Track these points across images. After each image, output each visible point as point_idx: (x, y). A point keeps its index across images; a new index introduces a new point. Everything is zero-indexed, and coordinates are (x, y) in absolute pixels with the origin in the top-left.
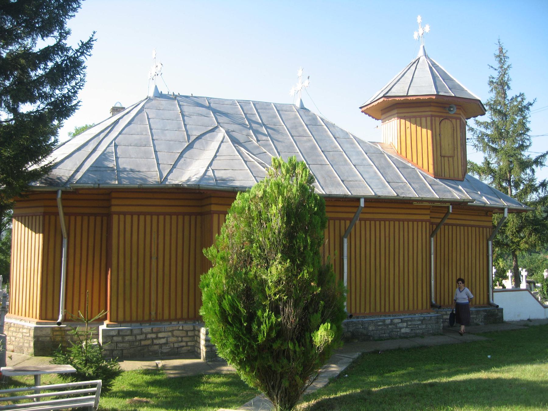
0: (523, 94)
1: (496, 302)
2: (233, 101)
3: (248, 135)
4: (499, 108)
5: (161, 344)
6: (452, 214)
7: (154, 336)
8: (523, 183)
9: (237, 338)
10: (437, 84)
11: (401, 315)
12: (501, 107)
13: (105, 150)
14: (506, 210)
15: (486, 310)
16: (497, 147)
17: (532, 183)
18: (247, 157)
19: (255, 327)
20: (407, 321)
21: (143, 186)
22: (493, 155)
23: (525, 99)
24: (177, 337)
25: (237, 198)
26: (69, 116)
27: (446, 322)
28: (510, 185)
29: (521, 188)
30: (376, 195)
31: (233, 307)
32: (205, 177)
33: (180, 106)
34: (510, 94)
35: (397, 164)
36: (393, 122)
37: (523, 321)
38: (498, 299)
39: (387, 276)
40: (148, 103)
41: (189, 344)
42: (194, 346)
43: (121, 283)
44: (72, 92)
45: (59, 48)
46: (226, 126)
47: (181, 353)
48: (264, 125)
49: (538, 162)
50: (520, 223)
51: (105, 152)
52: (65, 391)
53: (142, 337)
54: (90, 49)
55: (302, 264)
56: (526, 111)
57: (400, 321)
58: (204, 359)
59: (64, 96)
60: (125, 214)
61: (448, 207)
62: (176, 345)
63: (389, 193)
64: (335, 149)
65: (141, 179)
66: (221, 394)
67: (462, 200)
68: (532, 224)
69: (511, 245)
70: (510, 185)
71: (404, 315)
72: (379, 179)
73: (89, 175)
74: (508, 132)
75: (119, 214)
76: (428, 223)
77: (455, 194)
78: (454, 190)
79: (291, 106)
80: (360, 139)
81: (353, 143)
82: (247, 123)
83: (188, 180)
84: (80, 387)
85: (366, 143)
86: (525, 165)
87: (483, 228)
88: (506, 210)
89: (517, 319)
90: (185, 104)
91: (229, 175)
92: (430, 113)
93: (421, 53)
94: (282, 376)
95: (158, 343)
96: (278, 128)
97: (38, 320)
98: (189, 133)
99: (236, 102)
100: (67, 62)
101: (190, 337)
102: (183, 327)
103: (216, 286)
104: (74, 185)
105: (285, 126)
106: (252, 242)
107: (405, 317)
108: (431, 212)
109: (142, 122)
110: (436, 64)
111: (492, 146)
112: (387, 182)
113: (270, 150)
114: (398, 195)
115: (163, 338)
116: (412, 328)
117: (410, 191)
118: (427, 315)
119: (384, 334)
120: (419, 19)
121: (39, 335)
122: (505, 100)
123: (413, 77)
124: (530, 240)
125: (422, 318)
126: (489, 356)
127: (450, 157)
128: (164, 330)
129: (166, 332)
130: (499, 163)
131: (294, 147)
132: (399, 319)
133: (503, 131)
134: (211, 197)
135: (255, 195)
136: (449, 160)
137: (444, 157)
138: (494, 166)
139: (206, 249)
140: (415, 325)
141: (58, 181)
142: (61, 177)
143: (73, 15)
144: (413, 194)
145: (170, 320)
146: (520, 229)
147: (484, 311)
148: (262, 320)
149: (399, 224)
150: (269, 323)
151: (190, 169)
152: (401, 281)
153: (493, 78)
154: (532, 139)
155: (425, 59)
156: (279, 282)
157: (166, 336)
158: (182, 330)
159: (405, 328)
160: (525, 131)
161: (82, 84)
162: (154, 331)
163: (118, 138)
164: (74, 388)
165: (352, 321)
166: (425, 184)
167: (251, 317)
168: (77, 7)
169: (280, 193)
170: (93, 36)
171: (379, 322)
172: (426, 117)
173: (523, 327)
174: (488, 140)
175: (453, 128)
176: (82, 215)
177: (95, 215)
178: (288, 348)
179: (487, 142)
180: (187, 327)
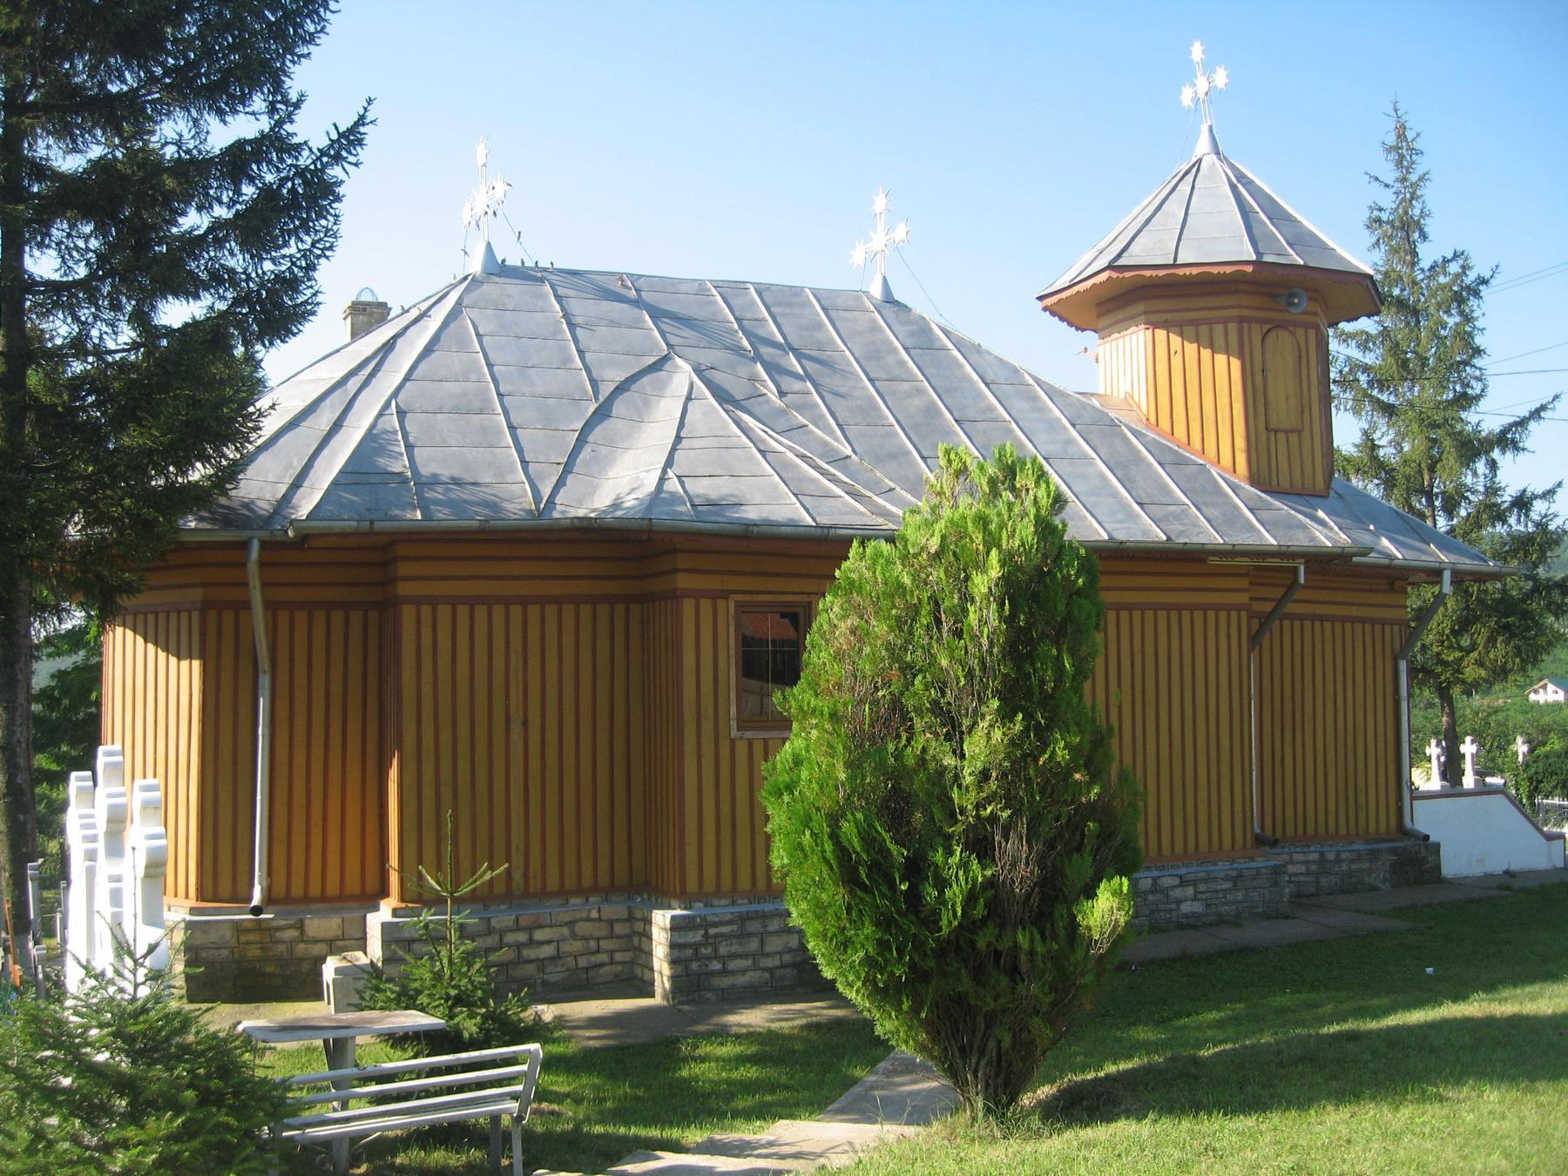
0: (1462, 253)
2: (701, 283)
3: (754, 379)
4: (1396, 292)
5: (542, 960)
6: (1304, 587)
7: (522, 937)
8: (1467, 498)
9: (884, 922)
11: (1178, 867)
14: (1447, 576)
17: (1493, 500)
18: (763, 441)
19: (931, 893)
20: (1194, 883)
22: (1382, 422)
23: (1470, 268)
25: (850, 555)
26: (289, 333)
28: (1431, 504)
29: (1463, 513)
30: (1111, 539)
31: (870, 840)
32: (663, 495)
33: (558, 297)
34: (1428, 254)
35: (1157, 453)
36: (1134, 336)
38: (1423, 819)
40: (472, 291)
41: (618, 957)
42: (631, 963)
43: (428, 793)
44: (300, 268)
45: (274, 143)
46: (688, 351)
48: (792, 349)
49: (1507, 439)
54: (358, 148)
56: (1473, 302)
57: (1176, 881)
58: (665, 996)
60: (433, 602)
61: (1295, 571)
62: (583, 962)
63: (1146, 532)
64: (989, 415)
65: (485, 504)
66: (748, 1087)
67: (1340, 550)
68: (1498, 611)
69: (1439, 669)
70: (1431, 504)
73: (340, 496)
74: (1424, 361)
75: (417, 601)
76: (1244, 614)
77: (1318, 534)
79: (858, 295)
80: (1052, 387)
81: (1034, 398)
82: (745, 343)
83: (616, 505)
84: (450, 1069)
85: (1068, 396)
86: (1473, 448)
87: (1313, 622)
88: (1447, 576)
89: (1477, 870)
90: (571, 293)
91: (725, 491)
92: (1236, 312)
93: (1203, 146)
94: (990, 1019)
95: (533, 956)
97: (192, 902)
98: (595, 375)
104: (304, 524)
106: (909, 670)
107: (1190, 870)
109: (463, 344)
110: (1246, 177)
111: (1378, 399)
112: (1138, 503)
113: (818, 420)
114: (1169, 539)
118: (1246, 866)
120: (1197, 52)
121: (198, 942)
122: (1413, 271)
123: (1186, 214)
124: (1492, 656)
125: (1234, 873)
126: (1429, 970)
127: (1292, 431)
130: (1399, 444)
131: (878, 409)
133: (1409, 355)
134: (674, 551)
136: (1288, 441)
137: (1276, 432)
138: (1386, 452)
139: (783, 693)
140: (1217, 891)
141: (246, 512)
142: (252, 502)
143: (306, 51)
144: (1212, 537)
145: (563, 893)
146: (1464, 624)
147: (1393, 851)
148: (945, 874)
150: (967, 883)
151: (611, 474)
152: (1177, 772)
153: (1380, 210)
154: (1492, 382)
155: (1217, 163)
157: (556, 938)
158: (599, 920)
160: (1472, 356)
161: (328, 245)
162: (522, 923)
163: (403, 391)
166: (1236, 507)
167: (916, 868)
168: (317, 32)
169: (992, 542)
170: (365, 109)
172: (1225, 322)
174: (1369, 382)
177: (347, 606)
178: (1016, 946)
179: (1365, 386)
180: (609, 911)
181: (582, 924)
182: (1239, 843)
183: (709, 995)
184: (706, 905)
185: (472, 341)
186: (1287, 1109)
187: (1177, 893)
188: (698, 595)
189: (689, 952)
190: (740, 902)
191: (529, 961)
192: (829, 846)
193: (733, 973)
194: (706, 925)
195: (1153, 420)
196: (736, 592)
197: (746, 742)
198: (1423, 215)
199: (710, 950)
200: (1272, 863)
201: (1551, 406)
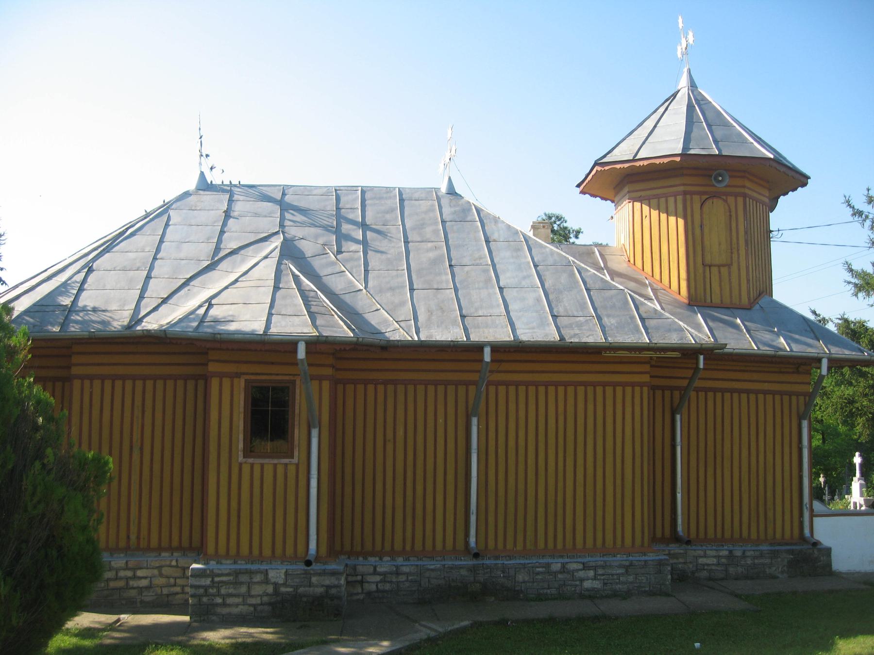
1: (819, 535)
5: (141, 588)
7: (129, 574)
20: (595, 568)
24: (168, 577)
27: (704, 569)
39: (560, 484)
47: (173, 605)
51: (69, 282)
57: (581, 566)
60: (91, 378)
62: (165, 591)
65: (103, 323)
71: (592, 557)
75: (82, 378)
76: (645, 389)
91: (226, 314)
92: (681, 188)
93: (684, 82)
96: (387, 229)
102: (177, 561)
115: (145, 578)
116: (606, 581)
119: (549, 589)
123: (655, 126)
125: (627, 563)
126: (697, 645)
127: (723, 266)
128: (145, 565)
129: (151, 568)
132: (579, 562)
136: (720, 272)
137: (710, 266)
140: (612, 575)
145: (160, 549)
147: (791, 552)
157: (150, 575)
158: (177, 566)
159: (592, 579)
162: (130, 565)
165: (483, 564)
171: (538, 567)
172: (675, 195)
175: (728, 214)
181: (166, 568)
182: (638, 542)
183: (214, 618)
184: (217, 563)
187: (582, 574)
188: (221, 376)
189: (202, 591)
190: (239, 562)
191: (134, 588)
193: (229, 605)
194: (213, 575)
195: (632, 261)
196: (244, 374)
197: (249, 466)
199: (215, 590)
200: (657, 558)
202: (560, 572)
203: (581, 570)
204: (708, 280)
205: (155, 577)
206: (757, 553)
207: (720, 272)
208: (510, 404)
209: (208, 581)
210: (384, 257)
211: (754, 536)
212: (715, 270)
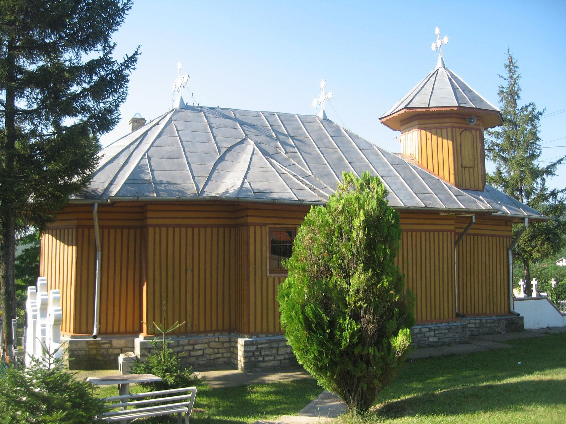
2: (258, 112)
3: (276, 147)
4: (509, 117)
6: (475, 224)
7: (191, 348)
8: (534, 192)
9: (321, 344)
10: (458, 96)
12: (511, 117)
13: (139, 163)
14: (526, 220)
15: (507, 319)
16: (507, 156)
18: (280, 170)
20: (434, 330)
21: (182, 198)
22: (503, 164)
23: (535, 109)
24: (213, 348)
25: (310, 211)
28: (521, 194)
29: (533, 197)
30: (405, 205)
31: (316, 315)
32: (243, 189)
33: (206, 117)
34: (520, 104)
35: (421, 175)
36: (414, 132)
37: (542, 329)
38: (517, 308)
41: (225, 355)
43: (157, 295)
44: (114, 106)
45: (105, 61)
46: (253, 137)
48: (290, 136)
49: (549, 171)
50: (532, 232)
51: (140, 165)
52: (143, 400)
53: (180, 349)
54: (135, 63)
55: (382, 272)
56: (536, 121)
57: (428, 330)
59: (106, 109)
60: (160, 226)
61: (471, 218)
62: (212, 357)
63: (417, 203)
64: (361, 161)
65: (179, 191)
66: (271, 403)
67: (488, 211)
69: (524, 254)
70: (521, 194)
72: (406, 190)
73: (127, 188)
75: (155, 226)
76: (453, 233)
77: (480, 204)
78: (478, 201)
79: (315, 117)
80: (384, 151)
81: (377, 155)
82: (273, 134)
83: (226, 192)
85: (390, 154)
86: (536, 174)
88: (526, 220)
89: (537, 327)
92: (450, 124)
93: (439, 64)
94: (359, 379)
95: (194, 355)
97: (72, 334)
98: (219, 145)
99: (261, 113)
100: (111, 76)
101: (226, 348)
103: (299, 295)
105: (310, 138)
106: (331, 253)
108: (455, 222)
109: (172, 134)
113: (299, 162)
114: (426, 206)
115: (200, 350)
117: (437, 201)
120: (437, 31)
121: (74, 348)
125: (449, 327)
126: (519, 363)
127: (471, 167)
129: (203, 344)
131: (321, 158)
133: (513, 140)
134: (247, 209)
135: (336, 209)
136: (469, 171)
137: (465, 168)
138: (505, 175)
140: (443, 334)
144: (441, 205)
145: (206, 332)
146: (533, 237)
147: (507, 319)
148: (343, 327)
149: (425, 234)
150: (351, 330)
151: (224, 181)
153: (503, 88)
155: (444, 71)
156: (358, 291)
158: (219, 341)
161: (123, 98)
163: (150, 150)
164: (152, 397)
166: (450, 195)
167: (333, 324)
168: (121, 21)
169: (361, 207)
170: (138, 49)
172: (447, 128)
173: (545, 335)
176: (115, 227)
177: (129, 228)
178: (369, 353)
183: (258, 369)
184: (257, 337)
185: (175, 132)
186: (467, 413)
187: (428, 334)
188: (255, 225)
189: (251, 354)
190: (269, 336)
192: (301, 316)
193: (267, 361)
194: (257, 344)
195: (420, 163)
198: (518, 90)
199: (258, 353)
200: (462, 323)
201: (564, 159)
202: (419, 334)
203: (428, 332)
204: (464, 175)
205: (206, 348)
206: (492, 321)
207: (469, 171)
208: (188, 246)
209: (254, 348)
210: (311, 156)
211: (488, 312)
212: (467, 169)
